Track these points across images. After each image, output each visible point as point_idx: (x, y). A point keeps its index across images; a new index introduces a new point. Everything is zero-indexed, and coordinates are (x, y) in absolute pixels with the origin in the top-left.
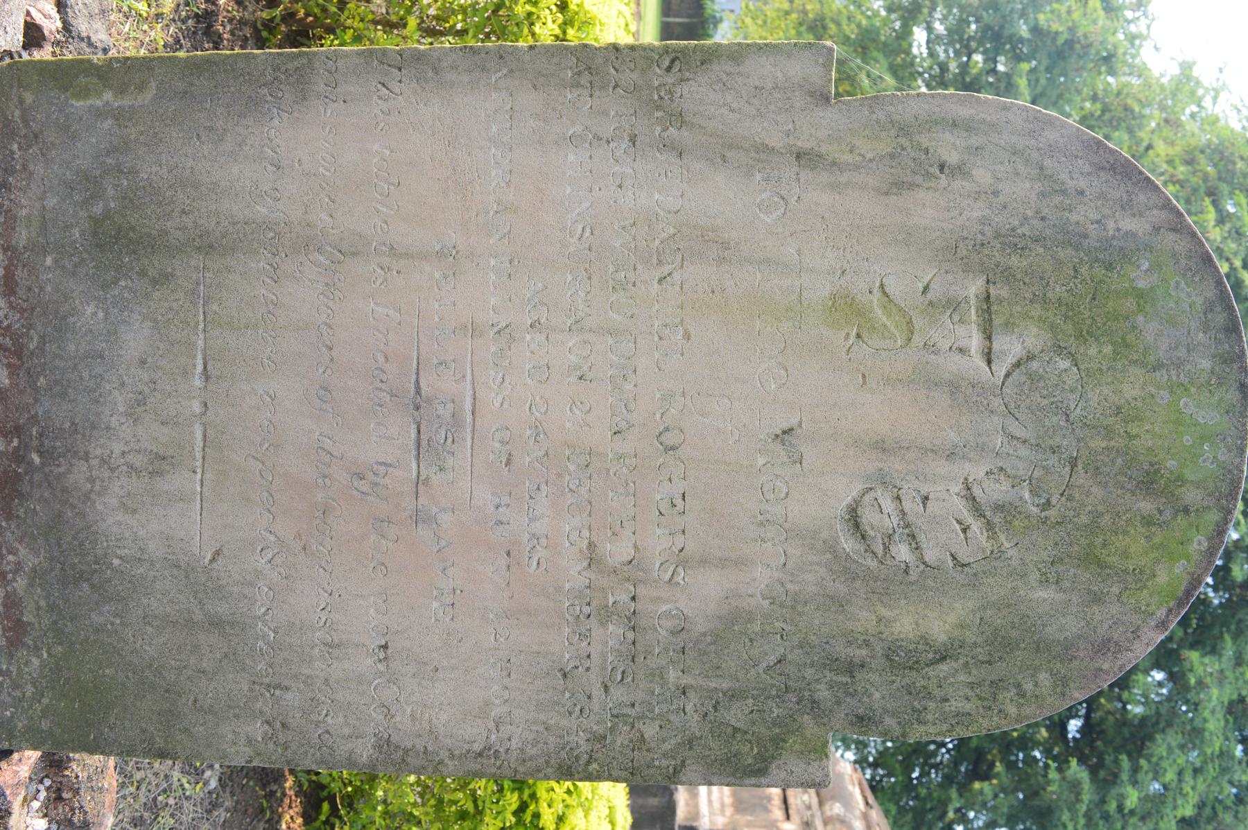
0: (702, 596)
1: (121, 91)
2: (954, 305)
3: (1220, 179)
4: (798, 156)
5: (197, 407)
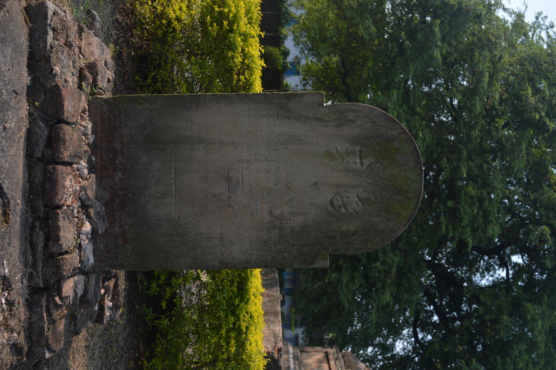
0: (297, 222)
2: (353, 153)
3: (535, 73)
4: (316, 119)
5: (173, 181)
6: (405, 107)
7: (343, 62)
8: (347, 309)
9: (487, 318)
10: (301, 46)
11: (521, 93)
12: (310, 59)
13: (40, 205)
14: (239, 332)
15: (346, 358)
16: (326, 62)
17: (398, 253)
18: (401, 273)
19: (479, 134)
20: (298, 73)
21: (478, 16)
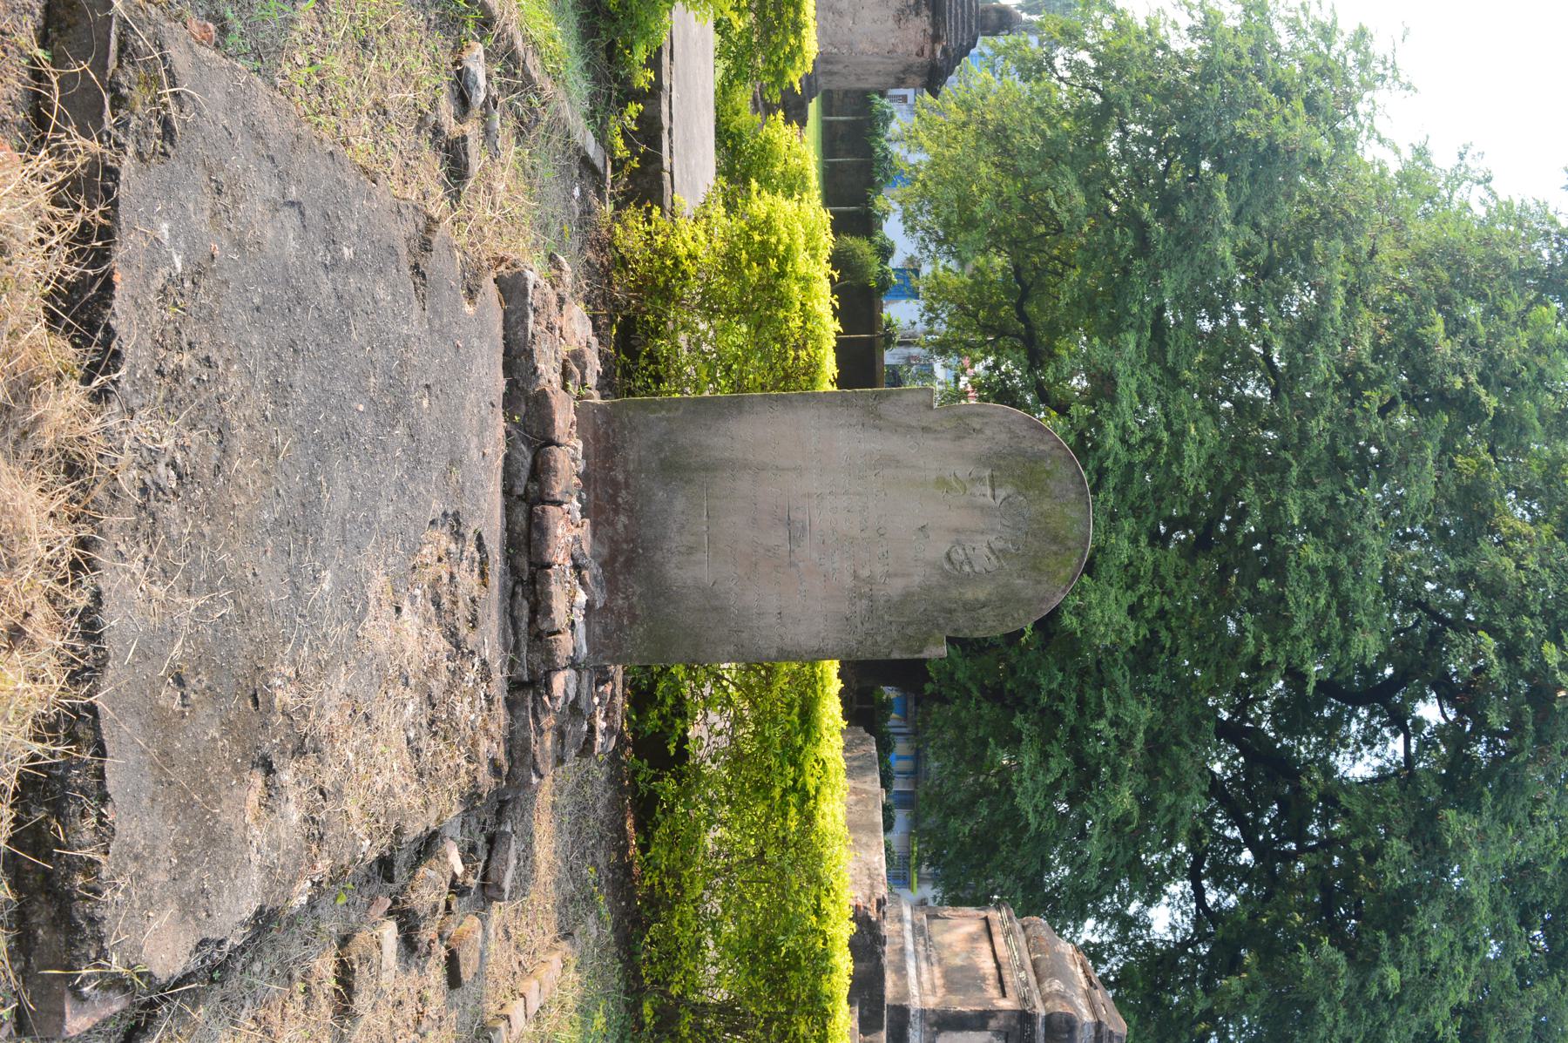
0: (896, 587)
1: (669, 410)
2: (980, 479)
3: (1453, 284)
6: (1156, 369)
7: (1018, 270)
8: (1033, 827)
9: (1356, 845)
10: (920, 234)
11: (1420, 330)
12: (942, 262)
13: (523, 562)
14: (805, 797)
15: (1030, 930)
16: (977, 269)
17: (1149, 700)
18: (1157, 745)
19: (1328, 426)
20: (915, 295)
21: (1315, 163)
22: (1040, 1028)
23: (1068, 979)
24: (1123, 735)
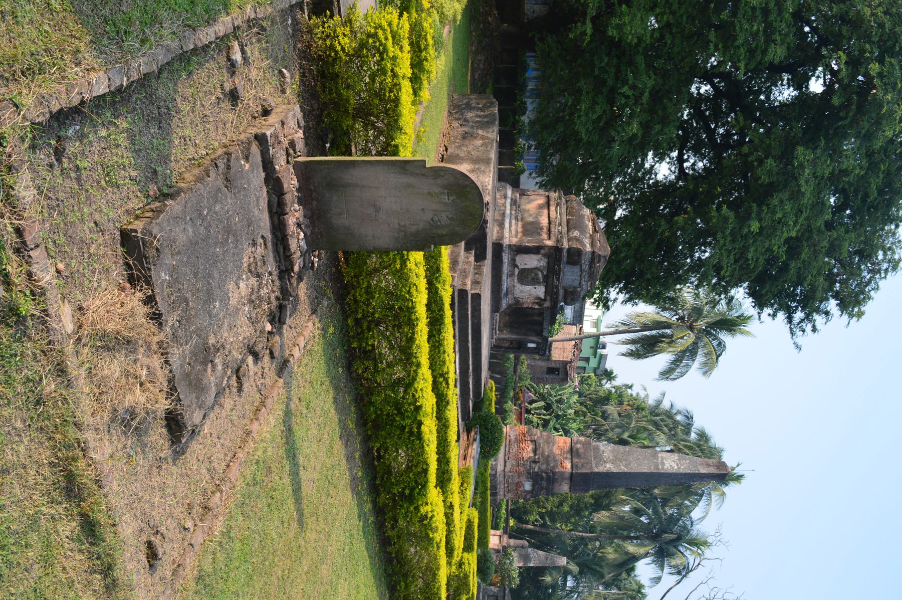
0: (413, 229)
22: (565, 253)
23: (582, 229)
24: (637, 94)
